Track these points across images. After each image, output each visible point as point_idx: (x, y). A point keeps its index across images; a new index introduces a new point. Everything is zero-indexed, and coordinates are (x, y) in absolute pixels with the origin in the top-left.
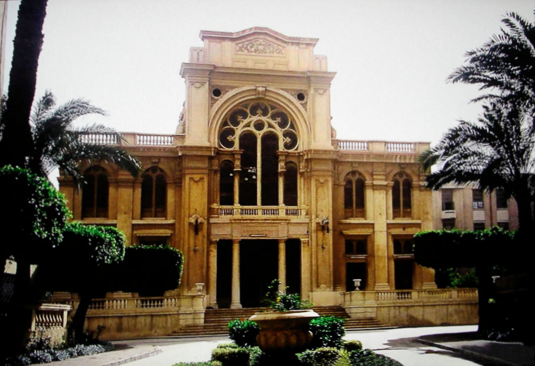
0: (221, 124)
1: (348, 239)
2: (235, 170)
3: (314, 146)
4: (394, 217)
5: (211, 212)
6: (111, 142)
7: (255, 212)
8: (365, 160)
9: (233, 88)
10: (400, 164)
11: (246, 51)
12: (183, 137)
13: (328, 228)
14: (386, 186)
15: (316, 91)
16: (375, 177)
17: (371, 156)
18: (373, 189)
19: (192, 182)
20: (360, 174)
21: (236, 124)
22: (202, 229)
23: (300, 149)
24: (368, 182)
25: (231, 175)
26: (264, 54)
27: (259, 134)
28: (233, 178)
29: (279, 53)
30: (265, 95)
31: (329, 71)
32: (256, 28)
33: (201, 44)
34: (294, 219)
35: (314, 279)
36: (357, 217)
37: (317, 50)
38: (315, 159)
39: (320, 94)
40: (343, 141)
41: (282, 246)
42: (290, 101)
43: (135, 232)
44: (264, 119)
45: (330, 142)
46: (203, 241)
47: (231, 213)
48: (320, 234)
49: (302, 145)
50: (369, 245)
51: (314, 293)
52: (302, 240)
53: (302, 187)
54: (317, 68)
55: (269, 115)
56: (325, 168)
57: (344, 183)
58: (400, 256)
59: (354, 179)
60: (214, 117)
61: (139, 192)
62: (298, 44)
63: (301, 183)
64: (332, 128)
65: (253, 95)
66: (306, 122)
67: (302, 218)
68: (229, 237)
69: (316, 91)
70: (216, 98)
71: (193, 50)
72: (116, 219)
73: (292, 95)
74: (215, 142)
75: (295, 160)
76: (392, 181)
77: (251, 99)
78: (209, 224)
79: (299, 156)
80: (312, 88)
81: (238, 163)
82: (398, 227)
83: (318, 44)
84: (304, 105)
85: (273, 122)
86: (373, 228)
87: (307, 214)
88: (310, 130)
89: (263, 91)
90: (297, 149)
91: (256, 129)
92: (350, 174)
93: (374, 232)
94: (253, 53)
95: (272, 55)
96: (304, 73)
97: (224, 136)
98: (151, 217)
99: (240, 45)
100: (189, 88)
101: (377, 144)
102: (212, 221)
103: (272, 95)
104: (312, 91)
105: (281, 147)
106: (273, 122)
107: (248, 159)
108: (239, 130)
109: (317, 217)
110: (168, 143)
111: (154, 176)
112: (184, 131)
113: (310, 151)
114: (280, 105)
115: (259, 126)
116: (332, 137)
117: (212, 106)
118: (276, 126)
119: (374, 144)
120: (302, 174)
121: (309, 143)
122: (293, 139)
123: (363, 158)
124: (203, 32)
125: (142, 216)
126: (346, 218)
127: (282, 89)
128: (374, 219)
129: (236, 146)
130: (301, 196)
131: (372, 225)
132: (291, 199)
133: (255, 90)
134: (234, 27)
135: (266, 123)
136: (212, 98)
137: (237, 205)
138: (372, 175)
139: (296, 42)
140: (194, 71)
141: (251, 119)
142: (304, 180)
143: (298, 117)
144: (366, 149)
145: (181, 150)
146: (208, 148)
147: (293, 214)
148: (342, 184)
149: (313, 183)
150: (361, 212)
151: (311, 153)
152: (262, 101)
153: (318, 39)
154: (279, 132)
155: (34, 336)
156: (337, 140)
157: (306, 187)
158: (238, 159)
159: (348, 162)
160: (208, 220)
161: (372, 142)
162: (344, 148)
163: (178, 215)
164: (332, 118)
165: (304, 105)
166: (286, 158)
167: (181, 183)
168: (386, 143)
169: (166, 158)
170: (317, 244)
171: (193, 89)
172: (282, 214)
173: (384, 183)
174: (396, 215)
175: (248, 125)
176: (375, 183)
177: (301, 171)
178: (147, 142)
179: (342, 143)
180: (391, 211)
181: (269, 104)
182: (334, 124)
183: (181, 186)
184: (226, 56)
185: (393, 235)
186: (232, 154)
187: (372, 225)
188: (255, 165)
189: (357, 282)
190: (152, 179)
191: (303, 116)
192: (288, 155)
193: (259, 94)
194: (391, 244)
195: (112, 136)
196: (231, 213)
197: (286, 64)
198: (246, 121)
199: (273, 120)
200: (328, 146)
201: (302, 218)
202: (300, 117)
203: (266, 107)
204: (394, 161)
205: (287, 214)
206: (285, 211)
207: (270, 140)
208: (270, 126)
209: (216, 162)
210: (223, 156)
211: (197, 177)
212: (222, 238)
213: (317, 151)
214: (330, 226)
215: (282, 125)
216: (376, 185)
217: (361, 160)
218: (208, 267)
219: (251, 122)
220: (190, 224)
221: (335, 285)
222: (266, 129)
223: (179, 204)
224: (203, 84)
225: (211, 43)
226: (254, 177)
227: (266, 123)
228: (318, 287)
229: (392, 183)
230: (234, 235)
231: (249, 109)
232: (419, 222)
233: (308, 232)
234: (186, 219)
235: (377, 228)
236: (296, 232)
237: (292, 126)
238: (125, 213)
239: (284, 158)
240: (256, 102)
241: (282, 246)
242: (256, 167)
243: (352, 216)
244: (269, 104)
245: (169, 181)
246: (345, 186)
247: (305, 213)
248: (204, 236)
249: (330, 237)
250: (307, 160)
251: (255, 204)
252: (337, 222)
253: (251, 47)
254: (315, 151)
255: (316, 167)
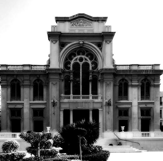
0: (64, 60)
1: (120, 109)
2: (71, 79)
3: (105, 67)
4: (141, 100)
5: (60, 97)
6: (150, 68)
7: (79, 98)
8: (128, 73)
9: (69, 43)
10: (145, 75)
11: (75, 26)
12: (49, 66)
13: (110, 104)
14: (138, 85)
15: (106, 42)
16: (133, 81)
17: (131, 71)
18: (132, 87)
19: (52, 85)
20: (126, 80)
21: (71, 59)
22: (56, 105)
23: (99, 69)
24: (130, 83)
25: (69, 82)
26: (83, 27)
27: (81, 63)
28: (70, 83)
29: (89, 26)
30: (83, 46)
31: (112, 31)
32: (79, 14)
33: (55, 24)
34: (96, 100)
35: (104, 127)
36: (124, 100)
37: (107, 23)
38: (105, 73)
39: (108, 43)
40: (118, 65)
41: (91, 113)
42: (94, 47)
43: (31, 106)
44: (83, 57)
45: (112, 65)
46: (57, 110)
47: (69, 98)
48: (107, 107)
49: (100, 67)
50: (129, 113)
51: (104, 133)
52: (99, 110)
53: (100, 86)
54: (107, 31)
55: (85, 55)
56: (109, 77)
57: (119, 84)
58: (144, 117)
59: (123, 83)
60: (62, 56)
61: (32, 89)
62: (98, 21)
63: (99, 85)
64: (113, 59)
65: (78, 46)
66: (102, 57)
67: (99, 100)
68: (68, 108)
69: (106, 42)
70: (62, 48)
71: (52, 26)
72: (23, 101)
73: (95, 45)
74: (62, 67)
75: (97, 75)
76: (141, 83)
77: (77, 48)
78: (60, 103)
79: (98, 72)
80: (104, 41)
81: (72, 76)
82: (143, 104)
83: (108, 20)
84: (101, 49)
85: (87, 58)
86: (132, 105)
87: (102, 98)
88: (103, 60)
89: (82, 44)
90: (97, 70)
91: (82, 61)
92: (121, 80)
93: (132, 106)
94: (78, 27)
95: (86, 27)
96: (100, 34)
97: (66, 64)
98: (38, 100)
99: (72, 23)
100: (50, 43)
101: (134, 66)
102: (61, 101)
103: (87, 45)
104: (104, 42)
105: (91, 68)
106: (87, 58)
107: (76, 75)
108: (72, 62)
109: (106, 99)
110: (43, 68)
111: (38, 83)
112: (49, 64)
113: (103, 69)
114: (90, 50)
115: (81, 60)
116: (113, 63)
117: (61, 52)
118: (88, 59)
119: (133, 66)
120: (99, 80)
121: (103, 66)
122: (96, 64)
123: (128, 72)
124: (56, 18)
125: (34, 100)
126: (119, 100)
127: (91, 42)
128: (132, 101)
129: (71, 69)
130: (99, 90)
131: (131, 103)
132: (95, 92)
133: (79, 43)
134: (69, 14)
135: (73, 52)
136: (60, 48)
137: (71, 95)
138: (131, 80)
139: (97, 20)
140: (52, 36)
141: (77, 57)
142: (100, 83)
143: (97, 55)
144: (129, 69)
145: (47, 71)
146: (59, 69)
147: (95, 98)
148: (117, 85)
149: (104, 84)
150: (126, 98)
151: (103, 70)
152: (82, 49)
153: (106, 18)
154: (90, 62)
155: (65, 98)
156: (116, 65)
157: (101, 86)
158: (72, 74)
159: (120, 75)
160: (59, 101)
161: (132, 65)
162: (119, 68)
163: (48, 99)
164: (113, 55)
165: (101, 49)
166: (92, 73)
167: (48, 85)
168: (139, 65)
169: (42, 75)
170: (106, 111)
171: (53, 44)
172: (91, 98)
173: (137, 84)
174: (142, 98)
175: (76, 60)
176: (133, 84)
177: (99, 79)
178: (35, 68)
179: (118, 66)
180: (140, 97)
181: (85, 50)
182: (114, 57)
183: (48, 87)
184: (66, 28)
185: (140, 108)
186: (69, 73)
187: (131, 103)
188: (79, 77)
189: (123, 128)
190: (37, 84)
191: (100, 54)
192: (93, 72)
193: (80, 45)
194: (140, 111)
195: (16, 67)
196: (69, 98)
197: (93, 30)
198: (75, 58)
199: (87, 57)
200: (112, 67)
201: (99, 100)
202: (99, 55)
203: (84, 51)
204: (142, 73)
205: (93, 98)
206: (92, 97)
207: (86, 65)
208: (86, 59)
209: (62, 76)
210: (66, 73)
211: (54, 83)
212: (65, 109)
213: (106, 69)
214: (112, 103)
215: (91, 59)
216: (133, 85)
217: (127, 74)
218: (59, 121)
219: (77, 58)
220: (52, 102)
221: (114, 129)
222: (84, 61)
223: (48, 94)
224: (56, 42)
225: (60, 23)
226: (79, 82)
227: (73, 52)
228: (106, 130)
229: (141, 84)
230: (70, 107)
231: (77, 52)
232: (153, 101)
233: (102, 106)
234: (50, 101)
235: (133, 104)
236: (97, 106)
237: (87, 51)
238: (27, 98)
239: (91, 73)
240: (80, 49)
241: (91, 113)
242: (80, 78)
243: (122, 100)
244: (85, 50)
245: (44, 84)
246: (119, 86)
247: (101, 98)
248: (57, 108)
249: (111, 108)
250: (101, 73)
251: (80, 94)
252: (115, 102)
253: (77, 24)
254: (105, 69)
255: (105, 77)
